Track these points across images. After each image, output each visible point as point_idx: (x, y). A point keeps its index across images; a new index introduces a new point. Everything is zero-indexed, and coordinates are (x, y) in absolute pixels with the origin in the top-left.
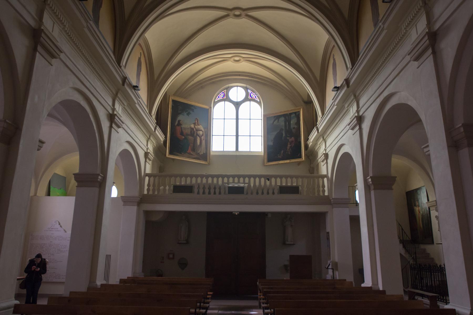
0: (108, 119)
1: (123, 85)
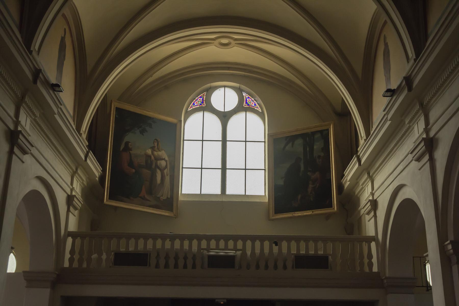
1: (35, 82)
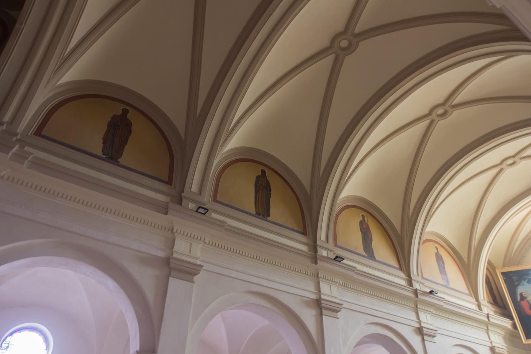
0: (417, 334)
1: (417, 296)
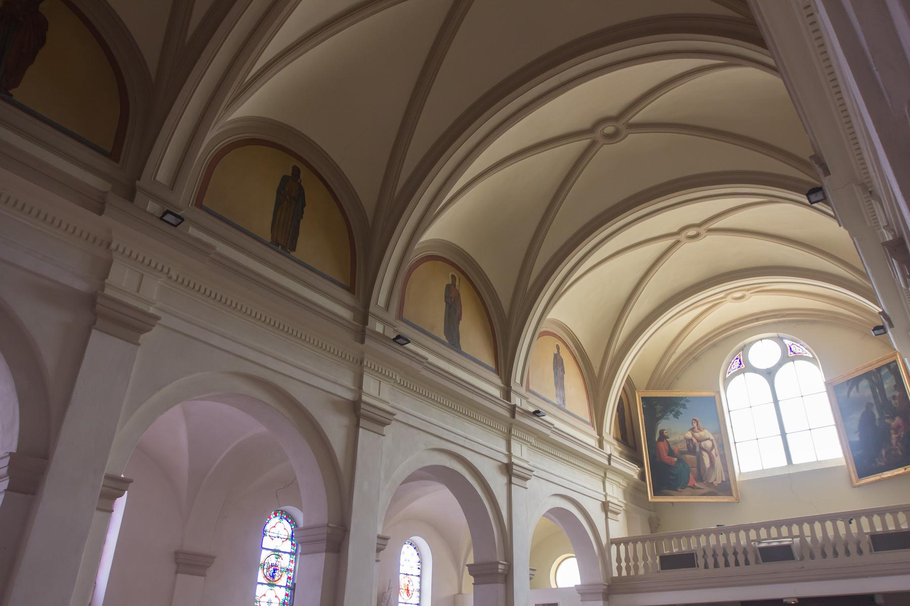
1: (513, 416)
